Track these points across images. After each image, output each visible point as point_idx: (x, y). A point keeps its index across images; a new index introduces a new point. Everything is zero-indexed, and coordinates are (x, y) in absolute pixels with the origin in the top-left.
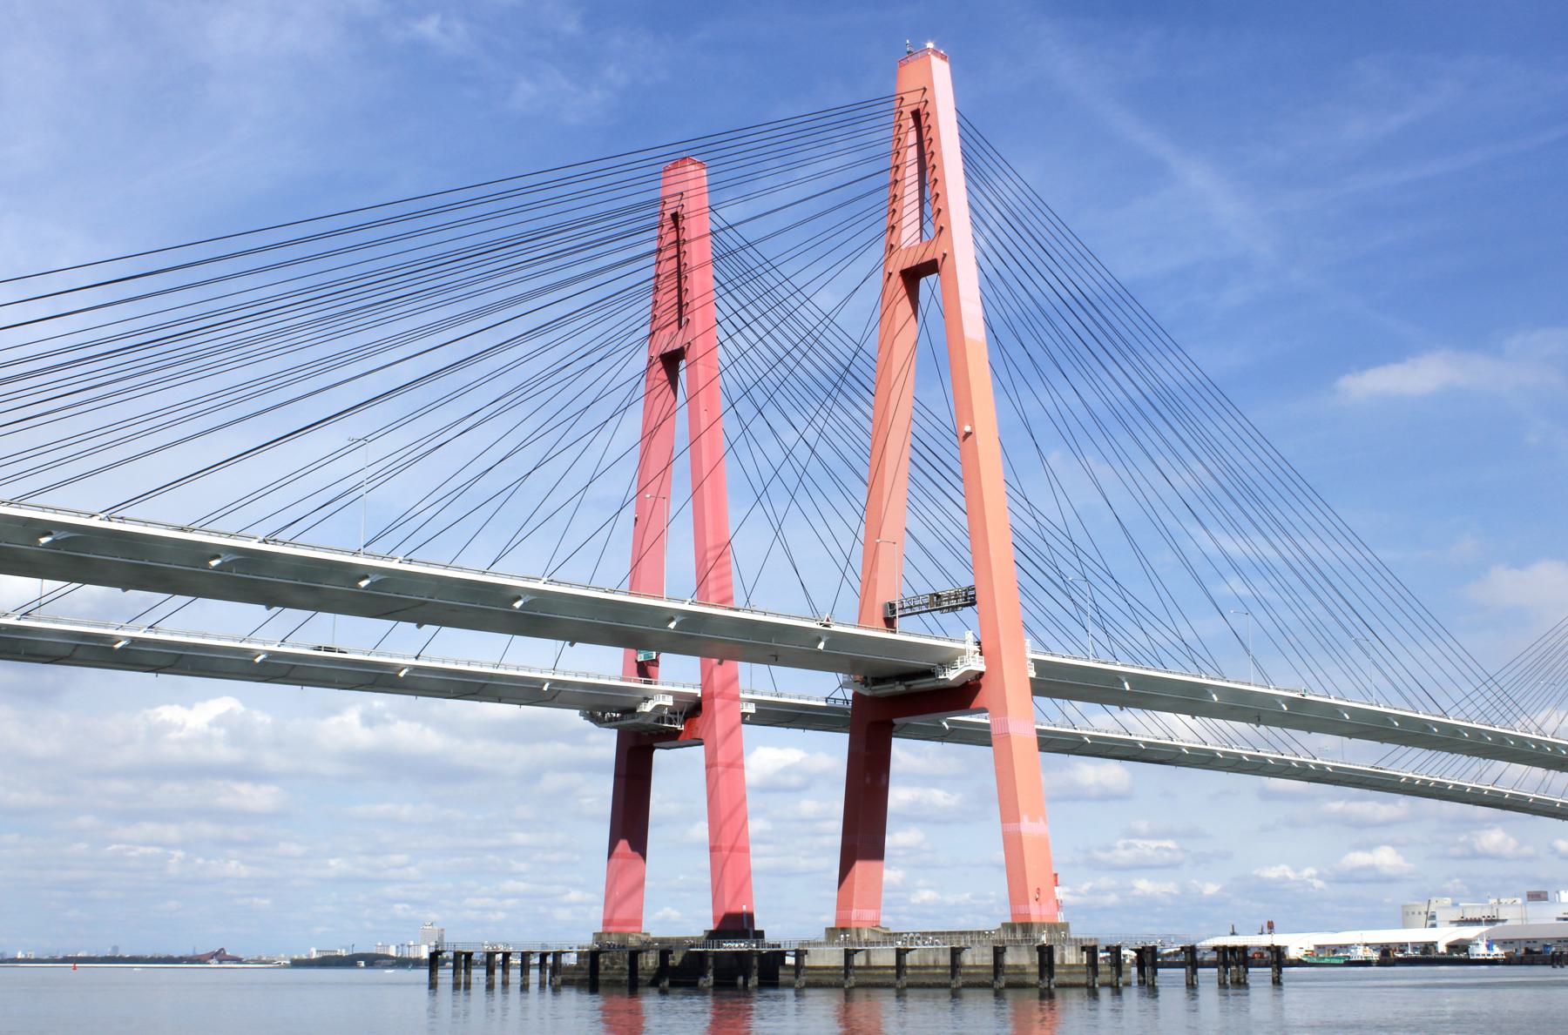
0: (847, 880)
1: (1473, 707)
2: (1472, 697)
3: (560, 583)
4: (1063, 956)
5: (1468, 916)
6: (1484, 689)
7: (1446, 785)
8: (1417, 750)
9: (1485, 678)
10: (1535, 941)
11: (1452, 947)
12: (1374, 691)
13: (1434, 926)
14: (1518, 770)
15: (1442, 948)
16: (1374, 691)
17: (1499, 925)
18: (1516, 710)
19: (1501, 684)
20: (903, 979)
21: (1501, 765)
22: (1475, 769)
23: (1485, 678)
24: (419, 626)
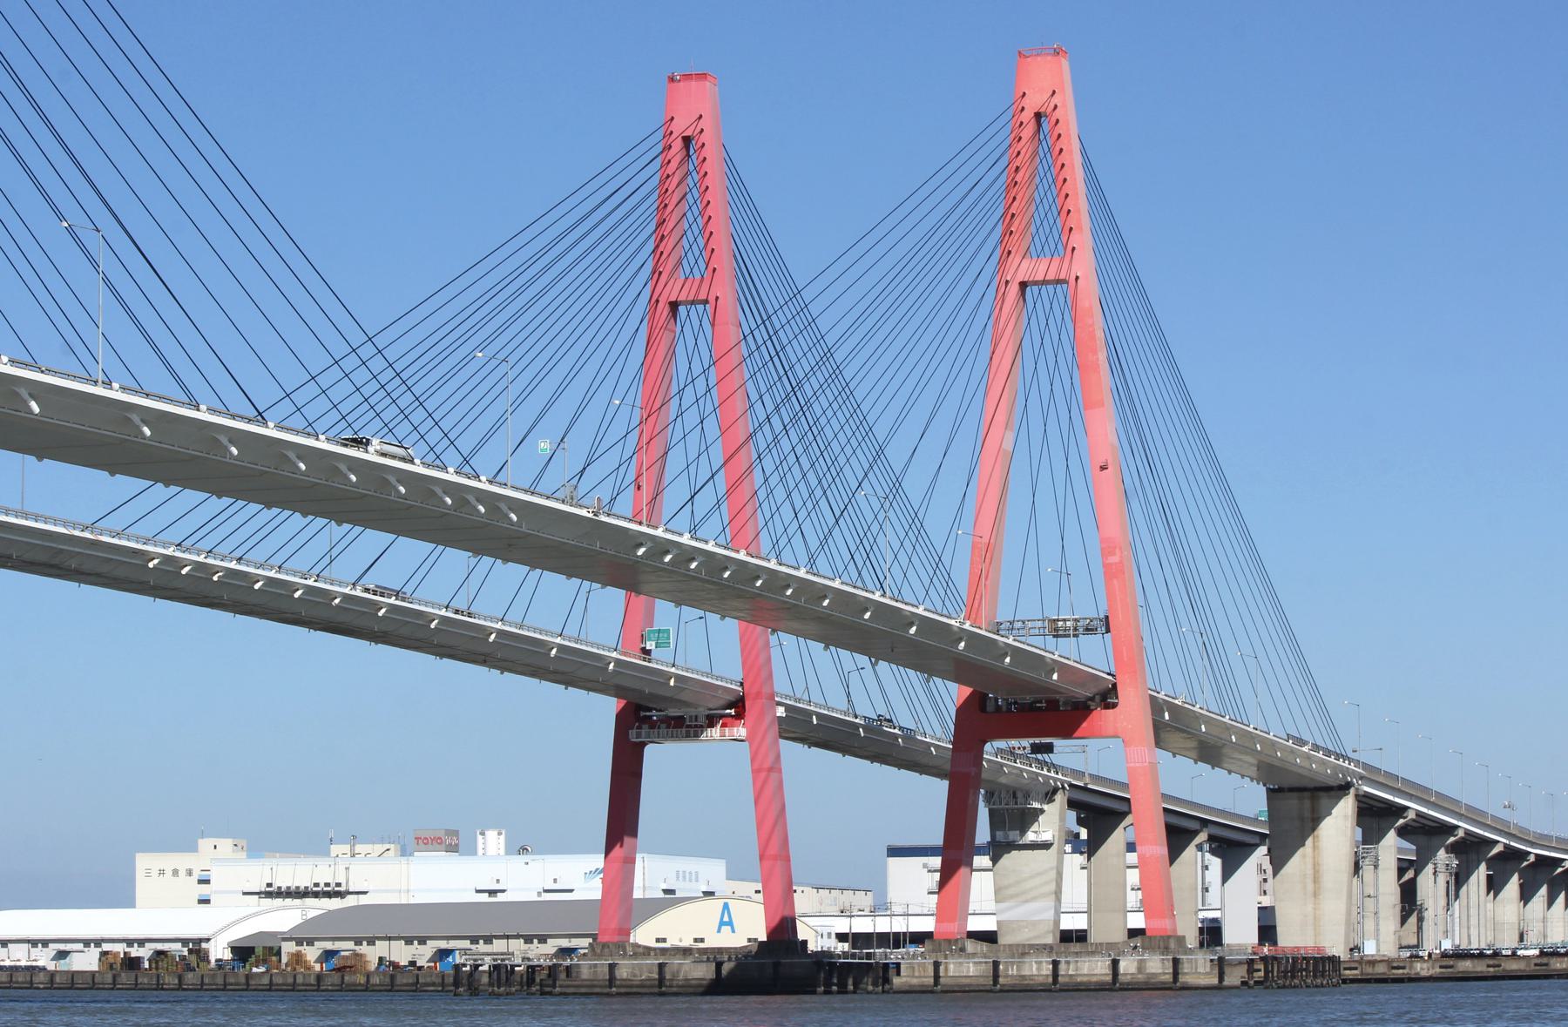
0: (952, 882)
1: (323, 404)
2: (324, 381)
3: (618, 517)
4: (946, 969)
5: (283, 882)
6: (350, 363)
7: (251, 579)
8: (192, 496)
9: (357, 338)
10: (142, 942)
11: (242, 952)
12: (101, 349)
13: (204, 901)
14: (556, 588)
15: (219, 951)
16: (101, 349)
17: (351, 901)
18: (418, 416)
19: (391, 354)
20: (632, 991)
21: (374, 539)
22: (320, 545)
23: (357, 338)
24: (723, 617)
